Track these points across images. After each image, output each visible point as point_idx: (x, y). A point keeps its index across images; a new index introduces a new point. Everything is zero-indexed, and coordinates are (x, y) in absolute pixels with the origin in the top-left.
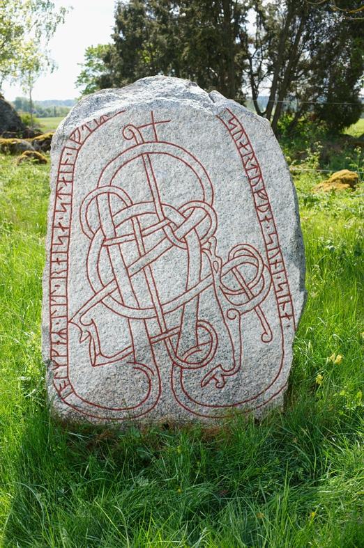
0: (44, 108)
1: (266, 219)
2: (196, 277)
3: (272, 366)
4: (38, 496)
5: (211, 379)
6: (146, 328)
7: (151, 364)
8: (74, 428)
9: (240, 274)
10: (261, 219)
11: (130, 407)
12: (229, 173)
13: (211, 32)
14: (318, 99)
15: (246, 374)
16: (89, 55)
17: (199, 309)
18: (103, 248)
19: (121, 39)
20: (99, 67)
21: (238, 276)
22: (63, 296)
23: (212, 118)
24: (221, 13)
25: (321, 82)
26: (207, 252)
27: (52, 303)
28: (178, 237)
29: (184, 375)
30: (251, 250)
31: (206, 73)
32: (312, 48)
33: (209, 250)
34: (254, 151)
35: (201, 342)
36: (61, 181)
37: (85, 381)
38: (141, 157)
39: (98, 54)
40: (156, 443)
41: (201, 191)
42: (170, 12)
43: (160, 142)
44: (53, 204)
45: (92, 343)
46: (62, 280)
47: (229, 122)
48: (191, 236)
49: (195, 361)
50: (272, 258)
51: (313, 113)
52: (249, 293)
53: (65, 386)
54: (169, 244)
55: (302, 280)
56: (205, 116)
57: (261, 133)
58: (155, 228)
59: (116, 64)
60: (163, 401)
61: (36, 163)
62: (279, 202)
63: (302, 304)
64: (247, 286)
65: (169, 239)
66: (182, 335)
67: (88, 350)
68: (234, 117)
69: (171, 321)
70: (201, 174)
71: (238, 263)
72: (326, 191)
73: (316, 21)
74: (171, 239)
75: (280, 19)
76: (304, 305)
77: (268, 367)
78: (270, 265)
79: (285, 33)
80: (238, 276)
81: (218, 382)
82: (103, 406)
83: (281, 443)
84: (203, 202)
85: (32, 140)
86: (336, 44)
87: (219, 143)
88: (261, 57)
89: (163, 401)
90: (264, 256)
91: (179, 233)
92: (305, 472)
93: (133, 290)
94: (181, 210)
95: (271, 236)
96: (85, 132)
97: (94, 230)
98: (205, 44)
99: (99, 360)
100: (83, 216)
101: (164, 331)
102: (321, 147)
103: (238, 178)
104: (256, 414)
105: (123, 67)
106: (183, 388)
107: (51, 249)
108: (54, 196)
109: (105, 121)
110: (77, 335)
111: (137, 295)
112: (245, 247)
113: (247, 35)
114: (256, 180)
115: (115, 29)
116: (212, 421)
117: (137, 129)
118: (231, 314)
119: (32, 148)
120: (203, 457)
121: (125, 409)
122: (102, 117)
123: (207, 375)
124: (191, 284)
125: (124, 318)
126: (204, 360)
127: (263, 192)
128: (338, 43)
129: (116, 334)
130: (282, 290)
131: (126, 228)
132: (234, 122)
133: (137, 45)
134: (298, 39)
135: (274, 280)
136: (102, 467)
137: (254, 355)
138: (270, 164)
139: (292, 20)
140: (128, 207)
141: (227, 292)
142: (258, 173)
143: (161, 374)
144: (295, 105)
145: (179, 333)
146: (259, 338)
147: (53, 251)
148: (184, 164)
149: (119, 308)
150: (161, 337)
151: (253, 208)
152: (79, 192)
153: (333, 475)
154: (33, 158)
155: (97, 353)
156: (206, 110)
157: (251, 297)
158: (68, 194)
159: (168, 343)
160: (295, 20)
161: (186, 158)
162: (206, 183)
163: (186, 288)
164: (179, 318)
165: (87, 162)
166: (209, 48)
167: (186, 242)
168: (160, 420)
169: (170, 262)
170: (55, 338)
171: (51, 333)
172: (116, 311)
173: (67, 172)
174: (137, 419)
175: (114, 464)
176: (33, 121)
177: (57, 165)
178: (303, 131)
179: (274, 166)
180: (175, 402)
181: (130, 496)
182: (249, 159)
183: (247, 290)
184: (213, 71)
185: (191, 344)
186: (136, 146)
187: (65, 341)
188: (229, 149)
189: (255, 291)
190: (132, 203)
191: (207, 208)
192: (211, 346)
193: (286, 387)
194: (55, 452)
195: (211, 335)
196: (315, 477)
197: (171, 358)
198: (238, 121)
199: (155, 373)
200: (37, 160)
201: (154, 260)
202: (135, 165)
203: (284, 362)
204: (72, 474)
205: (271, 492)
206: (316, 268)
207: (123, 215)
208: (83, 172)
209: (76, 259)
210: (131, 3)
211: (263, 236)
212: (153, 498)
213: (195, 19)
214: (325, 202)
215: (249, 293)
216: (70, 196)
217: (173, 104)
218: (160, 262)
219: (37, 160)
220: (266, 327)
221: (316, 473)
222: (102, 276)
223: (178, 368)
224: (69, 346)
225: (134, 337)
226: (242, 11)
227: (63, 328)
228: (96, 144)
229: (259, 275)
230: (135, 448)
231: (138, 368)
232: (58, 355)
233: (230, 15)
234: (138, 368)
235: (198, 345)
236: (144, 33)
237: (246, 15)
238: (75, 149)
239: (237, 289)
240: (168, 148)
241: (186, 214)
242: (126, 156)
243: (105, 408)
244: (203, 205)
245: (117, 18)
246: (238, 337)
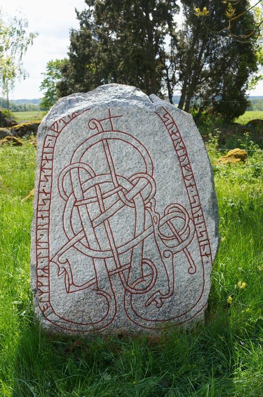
0: (17, 105)
1: (191, 185)
2: (141, 228)
3: (196, 291)
4: (32, 388)
5: (152, 301)
6: (106, 265)
7: (109, 291)
8: (55, 337)
9: (172, 225)
10: (187, 186)
11: (94, 322)
12: (164, 152)
13: (139, 50)
14: (216, 98)
15: (177, 297)
16: (50, 67)
17: (144, 251)
18: (74, 207)
19: (75, 56)
20: (58, 76)
21: (171, 226)
22: (46, 242)
23: (152, 113)
24: (146, 37)
25: (218, 86)
26: (149, 209)
27: (38, 247)
28: (128, 199)
29: (133, 299)
30: (181, 208)
31: (135, 80)
32: (210, 62)
33: (150, 208)
34: (182, 136)
35: (145, 274)
36: (44, 160)
37: (62, 303)
38: (101, 142)
39: (56, 66)
40: (116, 349)
41: (144, 165)
42: (109, 36)
43: (115, 131)
44: (39, 176)
45: (67, 276)
46: (45, 230)
47: (164, 116)
48: (137, 198)
49: (141, 288)
50: (195, 213)
51: (212, 107)
52: (179, 238)
53: (47, 307)
54: (122, 204)
55: (217, 229)
56: (147, 112)
57: (186, 124)
58: (112, 192)
59: (71, 74)
60: (118, 318)
61: (14, 145)
62: (200, 173)
63: (216, 246)
64: (178, 234)
65: (122, 201)
66: (131, 270)
67: (64, 281)
68: (168, 113)
69: (124, 260)
70: (144, 153)
71: (171, 217)
72: (224, 164)
73: (213, 43)
74: (123, 200)
75: (187, 41)
76: (218, 247)
77: (193, 292)
78: (194, 218)
79: (192, 51)
80: (171, 226)
81: (157, 303)
82: (75, 321)
83: (205, 347)
84: (146, 173)
85: (10, 128)
86: (227, 59)
87: (156, 131)
88: (174, 68)
89: (118, 318)
90: (189, 212)
91: (129, 196)
92: (223, 368)
93: (96, 237)
94: (130, 180)
95: (195, 197)
96: (61, 124)
97: (68, 195)
98: (135, 59)
99: (72, 288)
100: (60, 185)
101: (119, 266)
102: (220, 132)
103: (171, 156)
104: (186, 326)
105: (76, 76)
106: (132, 308)
107: (37, 208)
108: (40, 170)
109: (76, 116)
110: (56, 270)
111: (99, 241)
112: (176, 205)
113: (164, 53)
114: (183, 157)
115: (70, 49)
116: (153, 332)
117: (99, 122)
118: (167, 254)
119: (11, 134)
120: (151, 358)
121: (91, 324)
122: (73, 113)
123: (149, 298)
124: (138, 232)
125: (90, 258)
126: (147, 287)
127: (188, 166)
128: (229, 58)
129: (84, 270)
130: (202, 236)
131: (91, 193)
132: (168, 116)
133: (86, 60)
134: (201, 55)
135: (197, 229)
136: (78, 367)
137: (183, 283)
138: (193, 146)
139: (197, 41)
140: (92, 178)
141: (163, 238)
142: (185, 153)
143: (116, 298)
144: (199, 102)
145: (130, 268)
146: (187, 271)
147: (39, 210)
148: (132, 147)
149: (86, 251)
150: (117, 271)
151: (182, 178)
152: (57, 167)
153: (243, 369)
154: (12, 141)
155: (71, 283)
156: (148, 108)
157: (180, 241)
158: (50, 169)
159: (122, 275)
160: (198, 42)
161: (134, 142)
162: (148, 160)
163: (134, 235)
164: (129, 257)
165: (63, 146)
166: (138, 62)
167: (134, 203)
168: (117, 331)
169: (123, 217)
170: (40, 272)
171: (37, 269)
172: (84, 252)
173: (49, 153)
174: (99, 331)
175: (87, 364)
176: (9, 115)
177: (41, 148)
178: (205, 121)
179: (196, 147)
180: (127, 318)
181: (99, 387)
182: (178, 142)
183: (178, 237)
184: (140, 78)
185: (138, 276)
186: (98, 134)
187: (47, 275)
188: (164, 135)
189: (184, 237)
190: (95, 175)
191: (149, 178)
192: (153, 277)
193: (207, 306)
194: (43, 356)
195: (152, 269)
196: (229, 370)
197: (124, 286)
198: (170, 115)
199: (113, 297)
200: (15, 143)
201: (111, 216)
202: (98, 148)
203: (205, 288)
204: (56, 372)
205: (200, 383)
206: (222, 219)
207: (89, 183)
208: (60, 153)
209: (55, 216)
210: (82, 30)
211: (189, 197)
212: (115, 389)
213: (127, 42)
214: (224, 172)
215: (179, 238)
216: (51, 170)
217: (124, 104)
218: (115, 217)
219: (15, 143)
220: (192, 263)
221: (231, 368)
222: (74, 227)
223: (129, 293)
224: (50, 278)
225: (97, 271)
226: (161, 35)
227: (46, 265)
228: (70, 133)
229: (186, 226)
230: (100, 352)
231: (100, 294)
232: (42, 285)
233: (152, 39)
234: (100, 294)
235: (143, 277)
236: (91, 51)
237: (164, 38)
238: (54, 136)
239: (170, 236)
240: (121, 135)
241: (134, 182)
242: (90, 142)
243: (76, 323)
244: (146, 176)
245: (71, 41)
246: (172, 271)
